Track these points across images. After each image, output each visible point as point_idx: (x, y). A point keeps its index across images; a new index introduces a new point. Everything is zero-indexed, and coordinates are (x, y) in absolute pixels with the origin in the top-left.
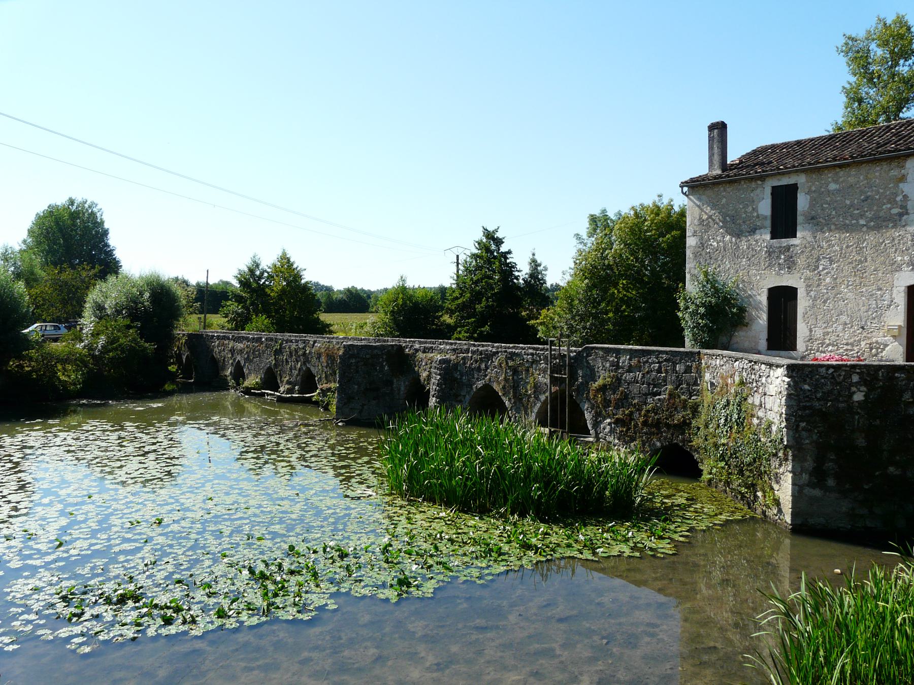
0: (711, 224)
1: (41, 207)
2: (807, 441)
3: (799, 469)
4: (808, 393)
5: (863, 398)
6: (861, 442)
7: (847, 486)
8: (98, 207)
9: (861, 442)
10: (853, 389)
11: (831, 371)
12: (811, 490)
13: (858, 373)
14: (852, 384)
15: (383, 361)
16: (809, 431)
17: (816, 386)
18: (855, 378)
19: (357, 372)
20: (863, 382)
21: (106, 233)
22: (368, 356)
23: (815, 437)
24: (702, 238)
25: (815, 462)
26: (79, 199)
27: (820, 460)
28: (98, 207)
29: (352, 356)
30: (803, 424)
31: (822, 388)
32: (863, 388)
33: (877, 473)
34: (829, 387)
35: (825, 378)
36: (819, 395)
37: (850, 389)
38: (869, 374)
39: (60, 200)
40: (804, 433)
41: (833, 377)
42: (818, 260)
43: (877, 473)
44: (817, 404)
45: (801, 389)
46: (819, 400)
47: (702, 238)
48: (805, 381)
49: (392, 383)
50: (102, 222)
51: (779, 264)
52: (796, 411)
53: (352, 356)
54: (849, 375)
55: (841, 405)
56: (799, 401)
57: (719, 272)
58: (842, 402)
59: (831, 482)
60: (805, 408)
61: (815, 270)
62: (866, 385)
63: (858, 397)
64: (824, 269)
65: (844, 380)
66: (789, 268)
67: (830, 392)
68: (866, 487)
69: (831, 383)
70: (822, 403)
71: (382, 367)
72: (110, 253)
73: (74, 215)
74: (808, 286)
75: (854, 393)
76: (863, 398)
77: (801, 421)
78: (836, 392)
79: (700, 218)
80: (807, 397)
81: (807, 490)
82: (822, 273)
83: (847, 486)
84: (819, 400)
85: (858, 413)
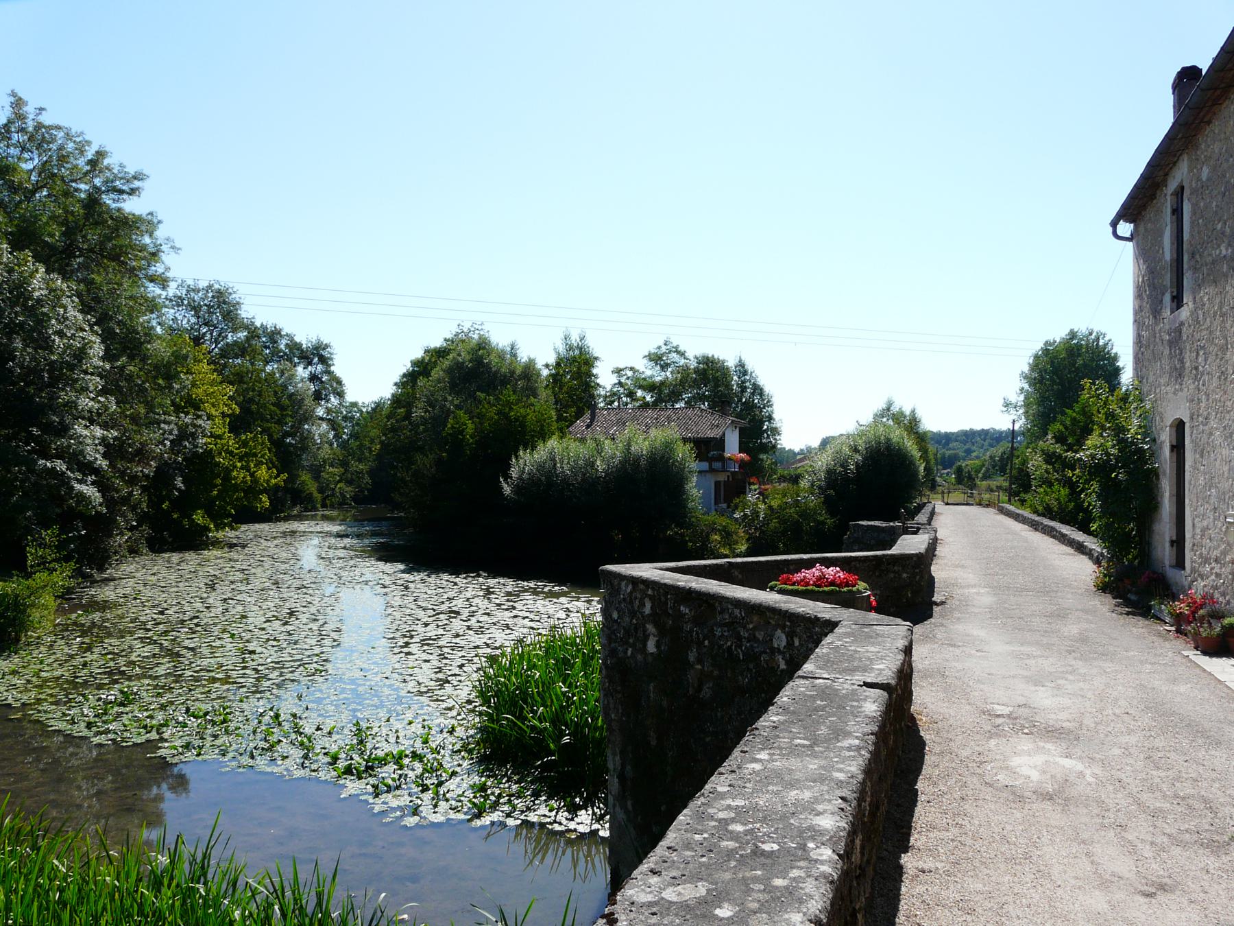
1: (1037, 346)
8: (1107, 339)
39: (1058, 334)
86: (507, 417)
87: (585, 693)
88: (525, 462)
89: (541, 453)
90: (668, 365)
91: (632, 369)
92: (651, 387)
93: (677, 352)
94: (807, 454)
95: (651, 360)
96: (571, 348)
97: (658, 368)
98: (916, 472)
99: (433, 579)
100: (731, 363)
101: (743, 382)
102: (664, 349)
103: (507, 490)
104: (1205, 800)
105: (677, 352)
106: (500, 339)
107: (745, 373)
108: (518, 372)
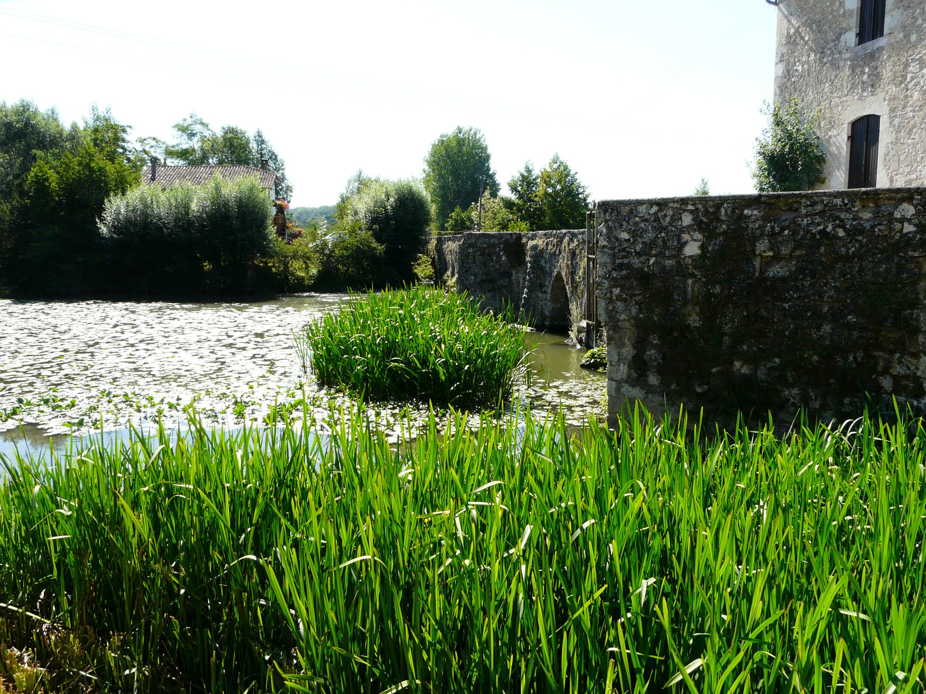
0: (798, 40)
1: (435, 138)
2: (623, 317)
3: (616, 358)
4: (626, 245)
5: (698, 252)
6: (694, 320)
7: (673, 387)
8: (481, 134)
9: (694, 320)
10: (686, 237)
11: (655, 209)
12: (630, 389)
13: (691, 212)
14: (682, 230)
15: (500, 251)
16: (625, 300)
17: (636, 233)
18: (687, 220)
19: (474, 262)
20: (698, 225)
21: (488, 158)
22: (485, 246)
23: (634, 311)
24: (788, 62)
25: (634, 348)
26: (466, 128)
27: (640, 344)
28: (481, 134)
29: (471, 246)
30: (617, 291)
31: (642, 237)
32: (698, 235)
33: (714, 370)
34: (651, 235)
35: (646, 220)
36: (639, 247)
37: (679, 236)
38: (706, 212)
39: (449, 130)
40: (619, 303)
41: (657, 220)
42: (907, 65)
43: (714, 370)
44: (636, 262)
45: (617, 239)
46: (638, 254)
47: (788, 62)
48: (621, 225)
49: (510, 275)
50: (486, 148)
51: (863, 83)
52: (610, 272)
53: (471, 246)
54: (676, 217)
55: (669, 263)
56: (614, 257)
57: (803, 108)
58: (669, 258)
59: (653, 380)
60: (620, 267)
61: (901, 82)
62: (701, 230)
63: (692, 249)
64: (912, 79)
65: (670, 224)
66: (872, 86)
67: (652, 244)
68: (699, 390)
69: (654, 228)
70: (643, 259)
71: (499, 257)
72: (491, 177)
73: (460, 142)
74: (892, 110)
75: (686, 243)
76: (698, 252)
77: (614, 286)
78: (660, 242)
79: (788, 33)
80: (624, 250)
81: (626, 388)
82: (910, 86)
83: (673, 387)
84: (638, 254)
85: (693, 275)
86: (88, 166)
87: (785, 3)
88: (116, 207)
89: (134, 195)
90: (194, 135)
91: (154, 139)
92: (184, 154)
93: (203, 124)
94: (310, 218)
95: (179, 129)
96: (98, 119)
97: (185, 136)
98: (428, 213)
99: (71, 305)
100: (251, 134)
101: (262, 150)
102: (189, 121)
103: (104, 230)
104: (706, 503)
105: (203, 124)
106: (42, 105)
107: (263, 142)
108: (65, 134)
